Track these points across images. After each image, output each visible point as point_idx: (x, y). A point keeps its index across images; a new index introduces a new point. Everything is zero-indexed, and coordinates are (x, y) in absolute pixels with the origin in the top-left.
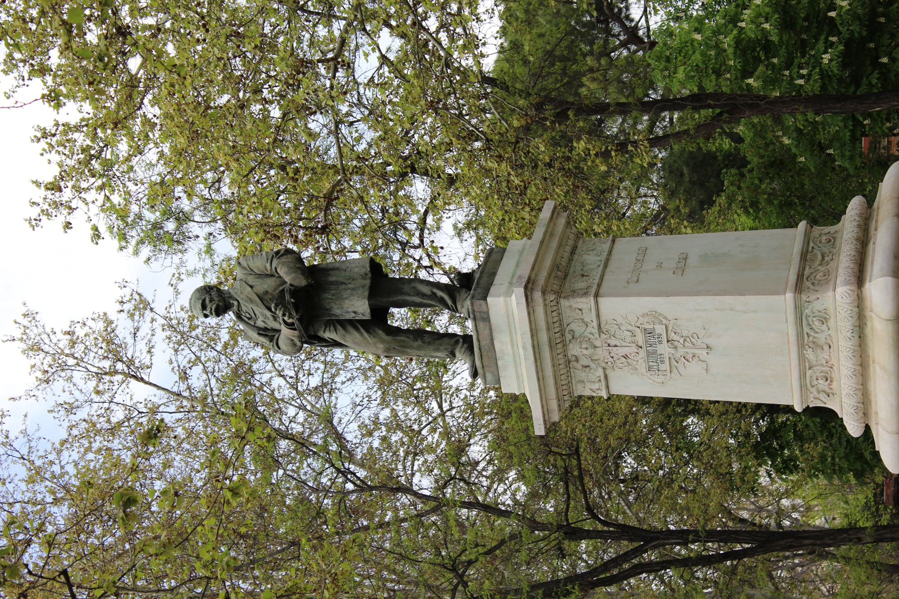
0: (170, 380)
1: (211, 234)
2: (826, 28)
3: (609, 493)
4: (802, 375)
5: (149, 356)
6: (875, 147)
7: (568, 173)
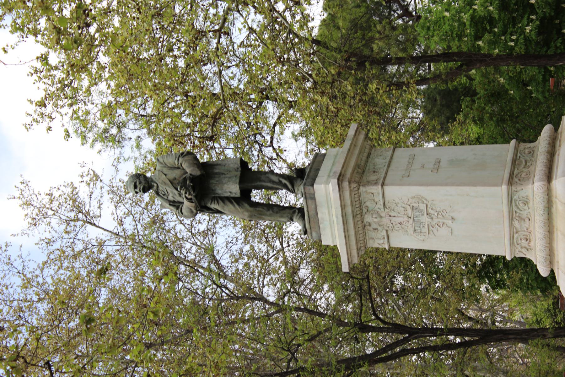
0: (112, 225)
1: (139, 137)
2: (528, 10)
3: (387, 301)
4: (512, 237)
5: (99, 210)
6: (558, 85)
7: (365, 103)
